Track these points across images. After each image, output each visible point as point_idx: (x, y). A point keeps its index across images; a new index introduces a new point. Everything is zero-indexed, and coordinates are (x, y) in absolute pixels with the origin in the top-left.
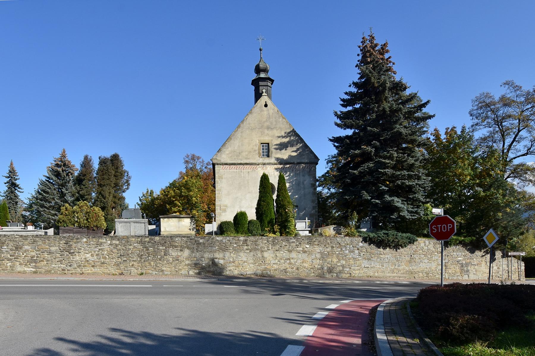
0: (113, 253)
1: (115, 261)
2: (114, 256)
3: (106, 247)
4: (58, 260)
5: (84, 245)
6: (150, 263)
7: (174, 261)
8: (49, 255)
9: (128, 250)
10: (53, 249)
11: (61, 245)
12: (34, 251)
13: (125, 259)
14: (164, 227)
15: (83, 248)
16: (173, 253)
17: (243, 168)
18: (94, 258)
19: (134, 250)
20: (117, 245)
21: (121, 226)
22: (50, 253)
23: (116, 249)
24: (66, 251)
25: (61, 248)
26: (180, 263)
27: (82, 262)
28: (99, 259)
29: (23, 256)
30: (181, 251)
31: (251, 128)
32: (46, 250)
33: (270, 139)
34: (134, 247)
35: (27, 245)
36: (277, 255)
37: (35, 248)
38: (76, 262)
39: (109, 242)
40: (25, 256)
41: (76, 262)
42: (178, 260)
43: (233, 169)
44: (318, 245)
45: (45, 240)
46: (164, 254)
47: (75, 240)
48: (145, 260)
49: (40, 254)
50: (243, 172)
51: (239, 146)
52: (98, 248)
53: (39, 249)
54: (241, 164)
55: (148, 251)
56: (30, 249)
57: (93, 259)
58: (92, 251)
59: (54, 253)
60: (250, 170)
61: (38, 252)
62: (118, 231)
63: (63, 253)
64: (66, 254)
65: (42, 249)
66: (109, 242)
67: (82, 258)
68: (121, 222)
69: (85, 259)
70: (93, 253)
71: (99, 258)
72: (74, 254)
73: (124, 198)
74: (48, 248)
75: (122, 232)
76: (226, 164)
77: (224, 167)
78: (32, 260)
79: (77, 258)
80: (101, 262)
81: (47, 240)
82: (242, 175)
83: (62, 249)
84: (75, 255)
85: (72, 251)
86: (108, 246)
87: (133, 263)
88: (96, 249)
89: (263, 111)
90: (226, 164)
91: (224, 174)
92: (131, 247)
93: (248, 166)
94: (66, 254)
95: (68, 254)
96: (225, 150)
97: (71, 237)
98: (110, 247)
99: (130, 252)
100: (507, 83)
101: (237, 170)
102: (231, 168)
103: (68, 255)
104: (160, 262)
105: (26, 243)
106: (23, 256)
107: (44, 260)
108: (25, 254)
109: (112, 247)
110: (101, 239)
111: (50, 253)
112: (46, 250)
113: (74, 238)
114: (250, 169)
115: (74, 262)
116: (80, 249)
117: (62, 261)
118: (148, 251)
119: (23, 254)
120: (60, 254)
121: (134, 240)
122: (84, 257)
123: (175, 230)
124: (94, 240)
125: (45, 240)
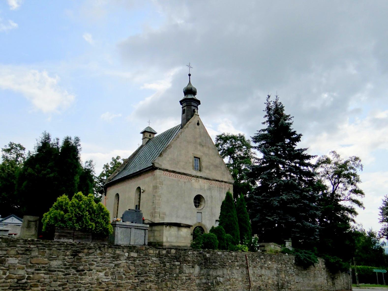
0: (129, 271)
1: (132, 283)
2: (131, 275)
3: (123, 261)
4: (59, 283)
5: (97, 258)
6: (166, 284)
7: (187, 280)
8: (47, 274)
9: (146, 267)
10: (55, 263)
11: (66, 258)
12: (23, 269)
13: (143, 279)
14: (166, 237)
15: (95, 263)
16: (187, 270)
17: (181, 177)
18: (108, 279)
19: (152, 266)
20: (134, 259)
21: (121, 232)
22: (50, 271)
23: (133, 265)
24: (73, 268)
25: (65, 262)
26: (192, 283)
27: (93, 285)
28: (114, 280)
29: (4, 276)
30: (193, 267)
31: (187, 141)
32: (44, 265)
33: (202, 154)
34: (153, 262)
35: (14, 257)
36: (255, 271)
37: (27, 262)
38: (85, 286)
39: (127, 254)
40: (7, 277)
41: (85, 286)
42: (190, 279)
43: (172, 176)
44: (275, 261)
45: (44, 249)
46: (179, 271)
47: (86, 251)
48: (162, 280)
49: (33, 273)
50: (181, 182)
51: (177, 155)
52: (114, 262)
53: (32, 265)
54: (179, 173)
55: (165, 268)
56: (18, 265)
57: (107, 280)
58: (106, 267)
59: (55, 271)
60: (186, 180)
61: (29, 270)
62: (117, 239)
63: (68, 270)
64: (72, 273)
65: (37, 264)
66: (127, 254)
67: (93, 279)
68: (122, 226)
69: (97, 279)
70: (107, 270)
71: (114, 278)
72: (84, 272)
73: (300, 137)
74: (46, 262)
75: (121, 240)
76: (167, 170)
77: (165, 173)
78: (18, 285)
79: (87, 279)
80: (116, 284)
81: (47, 249)
82: (180, 185)
83: (68, 264)
84: (85, 273)
85: (81, 268)
86: (126, 260)
87: (150, 284)
88: (111, 264)
89: (196, 128)
90: (167, 170)
91: (165, 180)
92: (149, 262)
93: (185, 176)
94: (72, 273)
95: (75, 272)
96: (165, 156)
97: (81, 246)
98: (128, 261)
99: (148, 269)
100: (333, 152)
101: (176, 179)
102: (171, 175)
103: (75, 274)
104: (175, 281)
105: (13, 252)
106: (4, 276)
107: (38, 285)
108: (8, 274)
109: (130, 262)
110: (118, 249)
111: (50, 271)
112: (44, 265)
113: (86, 247)
114: (186, 180)
115: (82, 286)
116: (92, 265)
117: (66, 284)
118: (165, 268)
119: (5, 274)
120: (63, 273)
121: (152, 252)
122: (96, 277)
123: (175, 241)
124: (110, 250)
125: (44, 249)
